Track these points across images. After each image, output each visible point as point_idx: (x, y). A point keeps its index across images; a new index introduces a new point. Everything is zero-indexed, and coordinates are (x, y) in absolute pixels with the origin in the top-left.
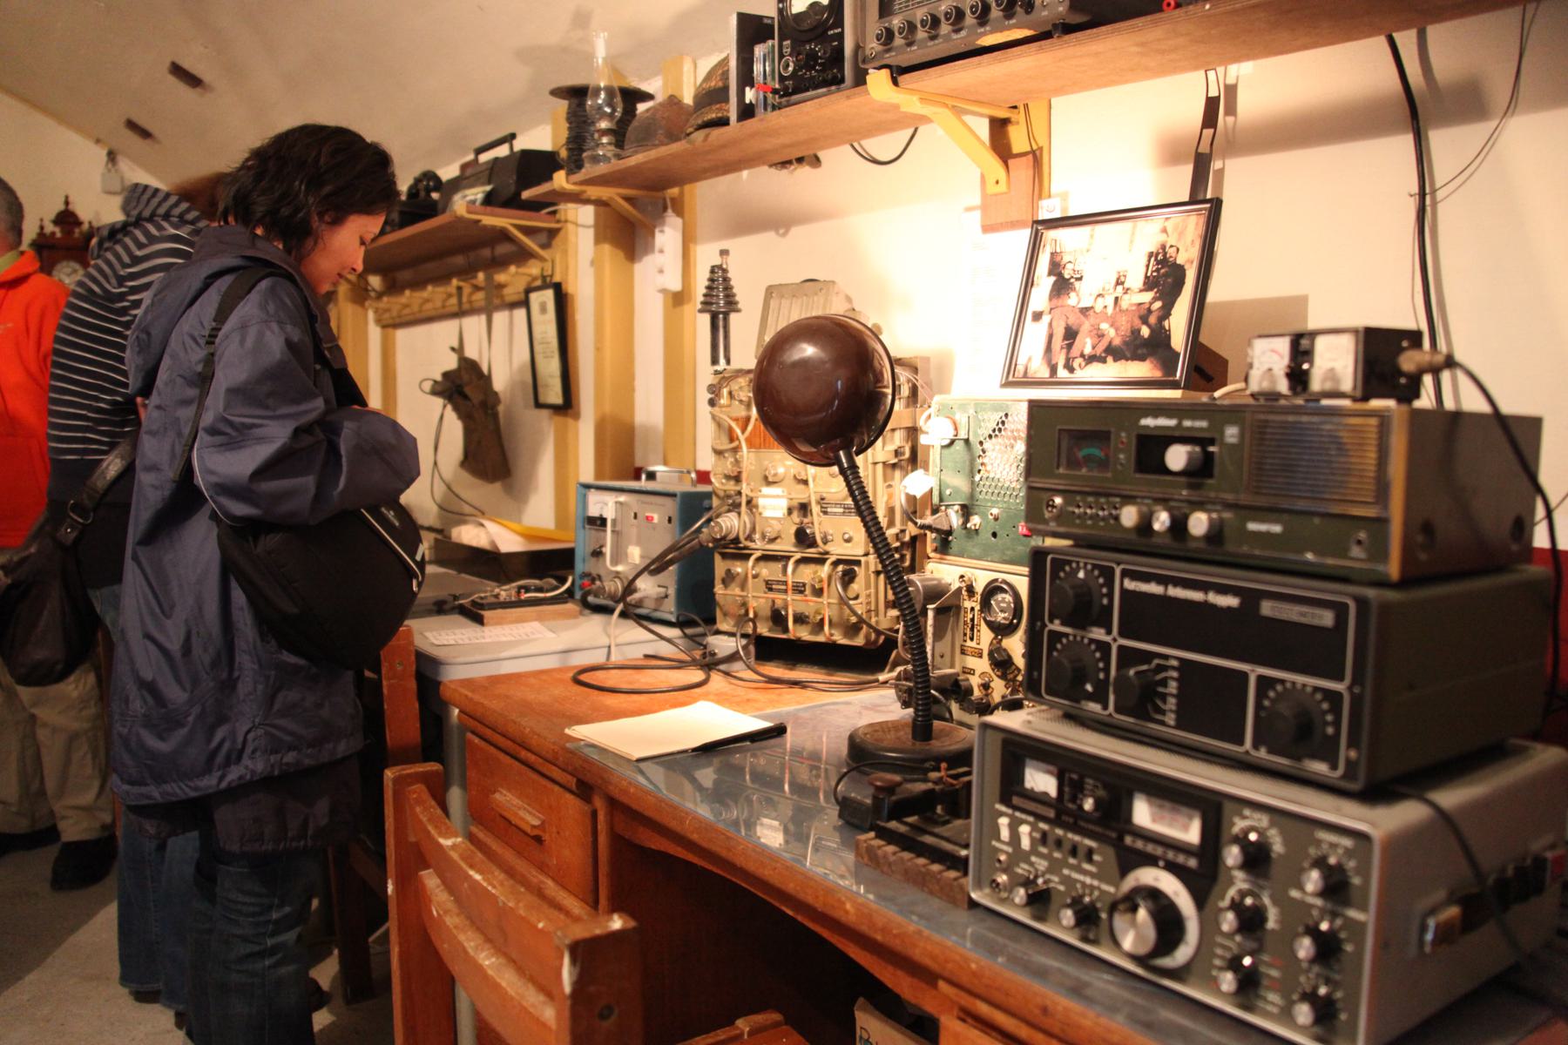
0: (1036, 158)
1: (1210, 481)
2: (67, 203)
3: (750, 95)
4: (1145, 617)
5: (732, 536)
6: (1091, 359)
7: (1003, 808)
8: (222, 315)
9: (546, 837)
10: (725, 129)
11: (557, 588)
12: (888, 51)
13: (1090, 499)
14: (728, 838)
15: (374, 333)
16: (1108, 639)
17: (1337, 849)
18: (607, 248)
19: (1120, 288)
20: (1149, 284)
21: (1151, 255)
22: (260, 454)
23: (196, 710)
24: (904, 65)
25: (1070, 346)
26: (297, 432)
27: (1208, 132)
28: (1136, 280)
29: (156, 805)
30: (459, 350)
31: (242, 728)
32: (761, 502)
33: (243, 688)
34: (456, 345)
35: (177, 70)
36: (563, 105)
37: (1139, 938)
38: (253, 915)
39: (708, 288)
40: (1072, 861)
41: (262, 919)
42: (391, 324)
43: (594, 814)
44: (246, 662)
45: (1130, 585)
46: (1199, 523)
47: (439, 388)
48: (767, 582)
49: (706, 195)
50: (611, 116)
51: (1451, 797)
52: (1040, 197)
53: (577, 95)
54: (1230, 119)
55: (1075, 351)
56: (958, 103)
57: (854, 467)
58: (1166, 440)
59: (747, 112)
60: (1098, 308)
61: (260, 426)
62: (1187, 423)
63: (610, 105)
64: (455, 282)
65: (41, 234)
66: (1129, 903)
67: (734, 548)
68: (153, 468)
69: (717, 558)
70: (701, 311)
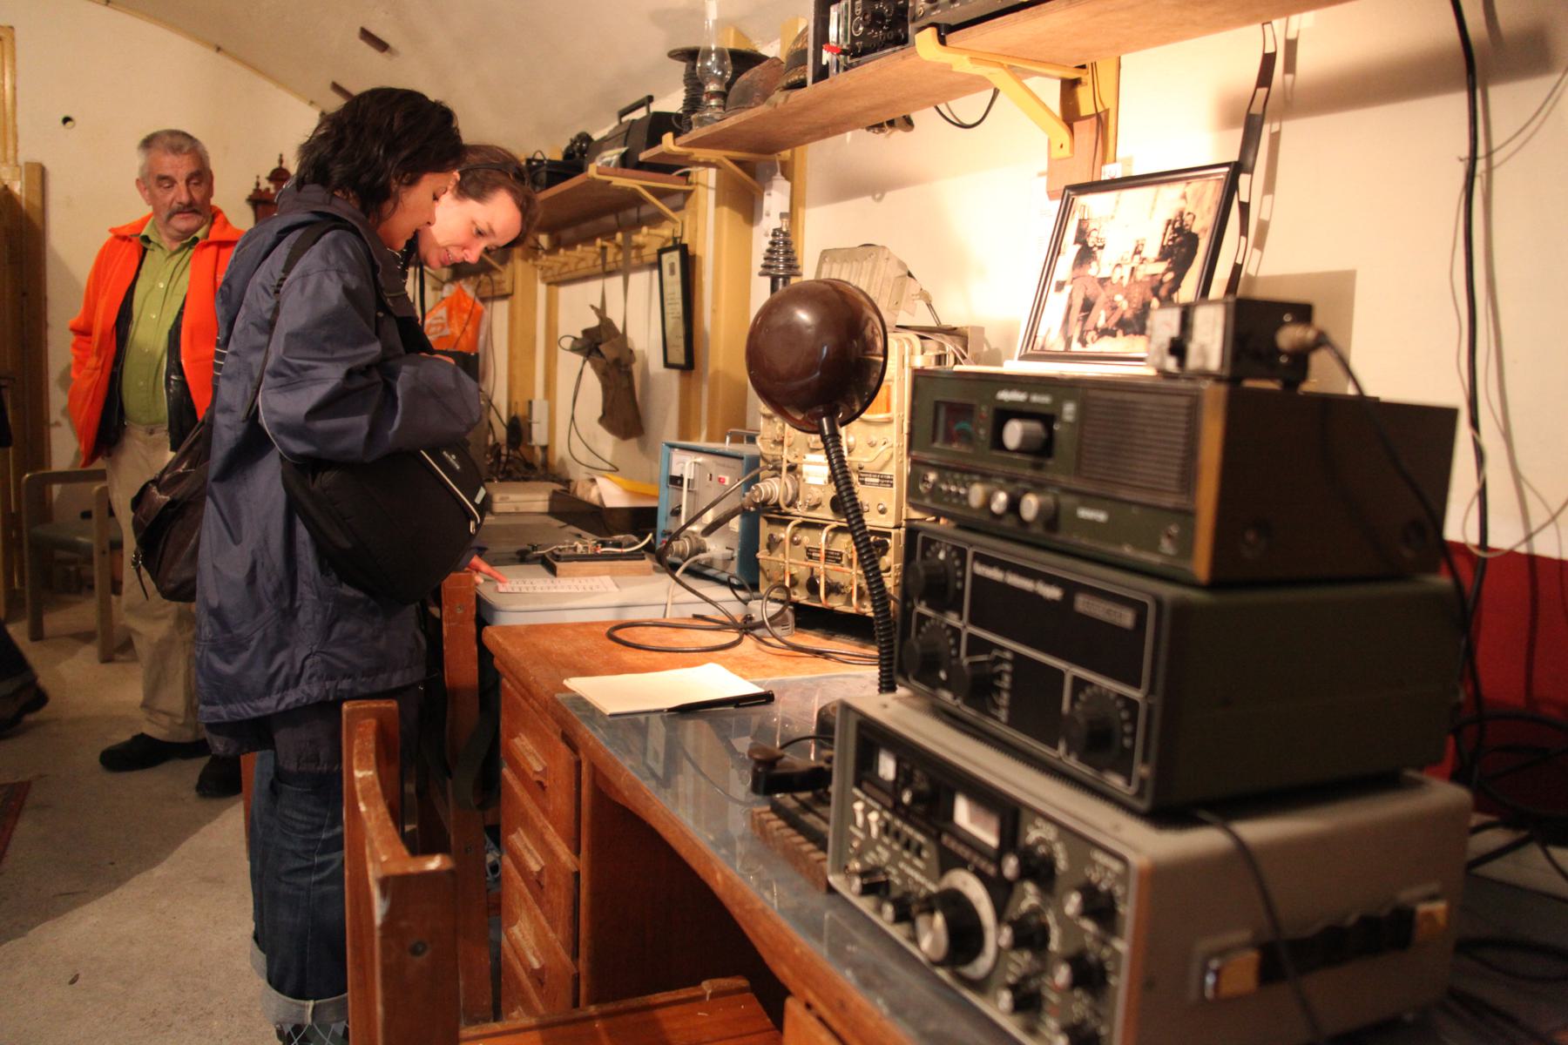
0: (1102, 122)
1: (1050, 462)
2: (281, 161)
3: (826, 57)
4: (997, 607)
5: (772, 502)
6: (1104, 332)
7: (857, 792)
8: (288, 269)
9: (547, 784)
10: (803, 91)
11: (635, 544)
12: (934, 9)
13: (957, 476)
14: (648, 798)
15: (542, 288)
16: (959, 624)
17: (1104, 872)
18: (725, 210)
19: (1137, 257)
20: (1165, 253)
21: (1169, 222)
22: (317, 393)
23: (258, 635)
24: (953, 22)
25: (1085, 318)
26: (350, 374)
27: (1262, 91)
28: (1152, 250)
29: (224, 724)
30: (601, 312)
31: (301, 654)
32: (805, 468)
33: (302, 617)
34: (598, 305)
35: (366, 35)
36: (681, 67)
37: (934, 942)
38: (305, 832)
39: (769, 251)
40: (907, 855)
41: (312, 837)
42: (556, 282)
43: (578, 764)
44: (306, 594)
45: (980, 569)
46: (1031, 505)
47: (578, 345)
48: (808, 550)
49: (817, 157)
50: (721, 79)
51: (1255, 831)
52: (1104, 162)
53: (690, 55)
54: (1289, 77)
55: (1089, 325)
56: (1019, 63)
57: (835, 436)
58: (1005, 414)
59: (822, 73)
60: (1115, 279)
61: (314, 368)
62: (1035, 398)
63: (720, 68)
64: (599, 242)
65: (257, 190)
66: (930, 904)
67: (774, 512)
68: (228, 410)
69: (763, 523)
70: (761, 274)
